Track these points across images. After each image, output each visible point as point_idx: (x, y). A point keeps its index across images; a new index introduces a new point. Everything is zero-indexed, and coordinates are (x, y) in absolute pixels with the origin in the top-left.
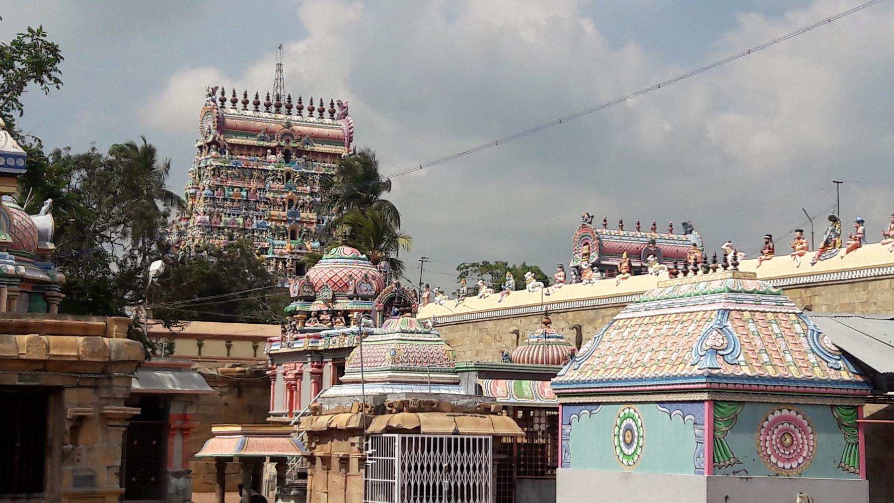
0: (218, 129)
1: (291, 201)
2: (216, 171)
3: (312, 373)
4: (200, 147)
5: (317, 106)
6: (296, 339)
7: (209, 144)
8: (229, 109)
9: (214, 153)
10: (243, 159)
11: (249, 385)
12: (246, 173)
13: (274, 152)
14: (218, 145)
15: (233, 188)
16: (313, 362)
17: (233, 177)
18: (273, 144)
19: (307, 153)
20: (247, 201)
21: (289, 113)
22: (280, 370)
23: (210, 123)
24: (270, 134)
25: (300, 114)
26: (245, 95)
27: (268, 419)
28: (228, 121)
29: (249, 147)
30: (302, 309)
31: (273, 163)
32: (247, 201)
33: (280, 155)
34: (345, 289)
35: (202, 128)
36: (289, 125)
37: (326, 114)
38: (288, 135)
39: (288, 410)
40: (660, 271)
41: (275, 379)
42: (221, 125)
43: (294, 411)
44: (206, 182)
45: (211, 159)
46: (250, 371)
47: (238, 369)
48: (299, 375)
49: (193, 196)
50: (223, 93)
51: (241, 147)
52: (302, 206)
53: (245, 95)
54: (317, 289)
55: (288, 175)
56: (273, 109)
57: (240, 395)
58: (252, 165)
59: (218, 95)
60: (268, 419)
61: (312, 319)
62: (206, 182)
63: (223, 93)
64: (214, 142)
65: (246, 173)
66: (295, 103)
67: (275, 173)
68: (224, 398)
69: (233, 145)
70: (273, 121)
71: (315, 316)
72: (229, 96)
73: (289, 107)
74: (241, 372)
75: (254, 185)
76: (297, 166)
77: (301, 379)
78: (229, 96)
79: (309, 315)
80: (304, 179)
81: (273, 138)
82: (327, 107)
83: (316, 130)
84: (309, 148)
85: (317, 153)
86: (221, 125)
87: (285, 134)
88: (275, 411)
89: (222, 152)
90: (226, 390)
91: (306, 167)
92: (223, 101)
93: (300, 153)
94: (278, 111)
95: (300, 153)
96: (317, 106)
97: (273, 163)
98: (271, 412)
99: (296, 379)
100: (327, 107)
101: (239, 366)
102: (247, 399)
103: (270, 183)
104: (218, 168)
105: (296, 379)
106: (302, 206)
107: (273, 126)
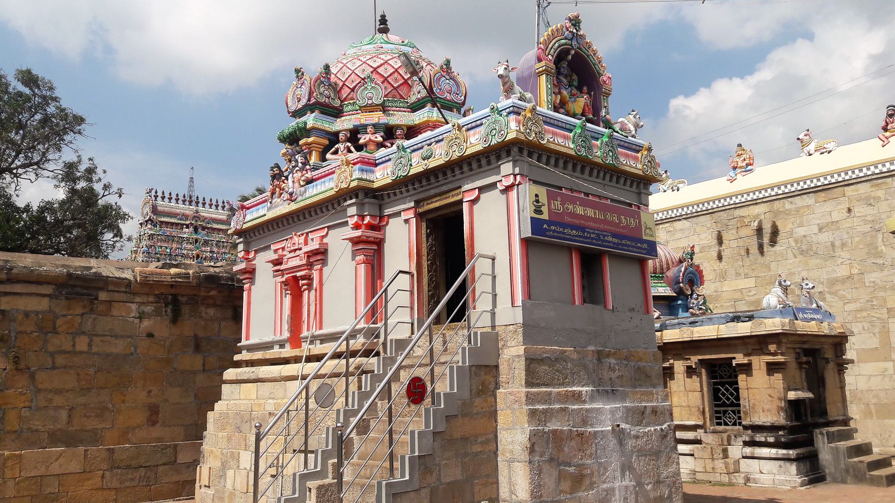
0: (152, 212)
1: (198, 256)
2: (151, 237)
3: (355, 241)
4: (141, 224)
5: (214, 202)
6: (309, 182)
7: (147, 221)
8: (159, 201)
9: (149, 226)
10: (168, 231)
11: (195, 301)
12: (170, 239)
13: (187, 227)
14: (152, 222)
15: (161, 247)
16: (362, 217)
17: (162, 241)
18: (188, 222)
19: (209, 228)
20: (170, 255)
21: (197, 206)
22: (262, 261)
23: (147, 209)
24: (186, 217)
25: (204, 206)
26: (170, 194)
27: (237, 358)
28: (159, 208)
29: (172, 224)
30: (319, 125)
31: (187, 233)
32: (170, 255)
33: (191, 229)
34: (403, 91)
35: (142, 213)
36: (197, 212)
37: (220, 208)
38: (197, 217)
39: (286, 335)
40: (680, 186)
41: (252, 280)
42: (154, 210)
43: (305, 333)
44: (144, 243)
45: (148, 230)
46: (197, 276)
47: (173, 271)
48: (320, 255)
49: (136, 252)
50: (156, 192)
51: (167, 223)
52: (205, 259)
53: (170, 194)
54: (345, 92)
55: (196, 241)
56: (187, 203)
57: (176, 318)
58: (174, 234)
59: (153, 193)
60: (237, 358)
61: (341, 146)
62: (144, 243)
63: (156, 192)
64: (149, 219)
65: (170, 239)
66: (201, 200)
67: (188, 239)
68: (146, 323)
69: (162, 222)
70: (189, 210)
71: (348, 140)
72: (160, 194)
73: (197, 203)
74: (178, 275)
75: (174, 246)
76: (202, 236)
77: (324, 262)
78: (160, 194)
79: (334, 138)
80: (206, 243)
81: (187, 219)
82: (220, 204)
83: (214, 216)
84: (209, 226)
85: (214, 229)
86: (154, 210)
87: (195, 217)
88: (253, 340)
89: (155, 226)
90: (148, 309)
91: (208, 236)
92: (156, 197)
93: (204, 228)
94: (190, 204)
95: (204, 228)
96: (214, 202)
97: (187, 233)
98: (244, 342)
99: (310, 265)
100: (220, 204)
101: (176, 266)
102: (188, 327)
103: (185, 245)
104: (152, 235)
105: (310, 265)
106: (205, 259)
107: (187, 212)
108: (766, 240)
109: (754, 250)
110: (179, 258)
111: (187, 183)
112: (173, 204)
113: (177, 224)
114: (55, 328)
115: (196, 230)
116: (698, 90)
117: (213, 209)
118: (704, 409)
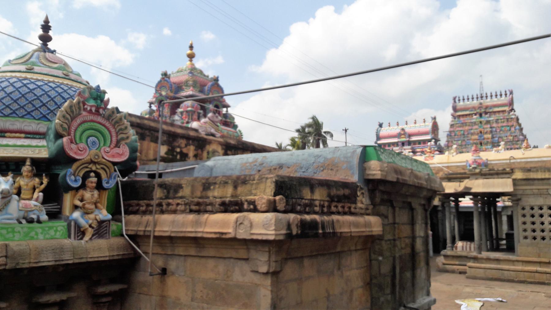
12: (464, 124)
13: (476, 114)
17: (458, 127)
19: (490, 112)
24: (474, 108)
31: (475, 118)
32: (464, 134)
65: (464, 124)
76: (485, 118)
84: (491, 110)
108: (67, 77)
109: (457, 100)
110: (470, 135)
111: (452, 101)
112: (494, 99)
113: (469, 115)
114: (264, 191)
115: (481, 115)
116: (31, 270)
117: (494, 99)
118: (62, 260)
